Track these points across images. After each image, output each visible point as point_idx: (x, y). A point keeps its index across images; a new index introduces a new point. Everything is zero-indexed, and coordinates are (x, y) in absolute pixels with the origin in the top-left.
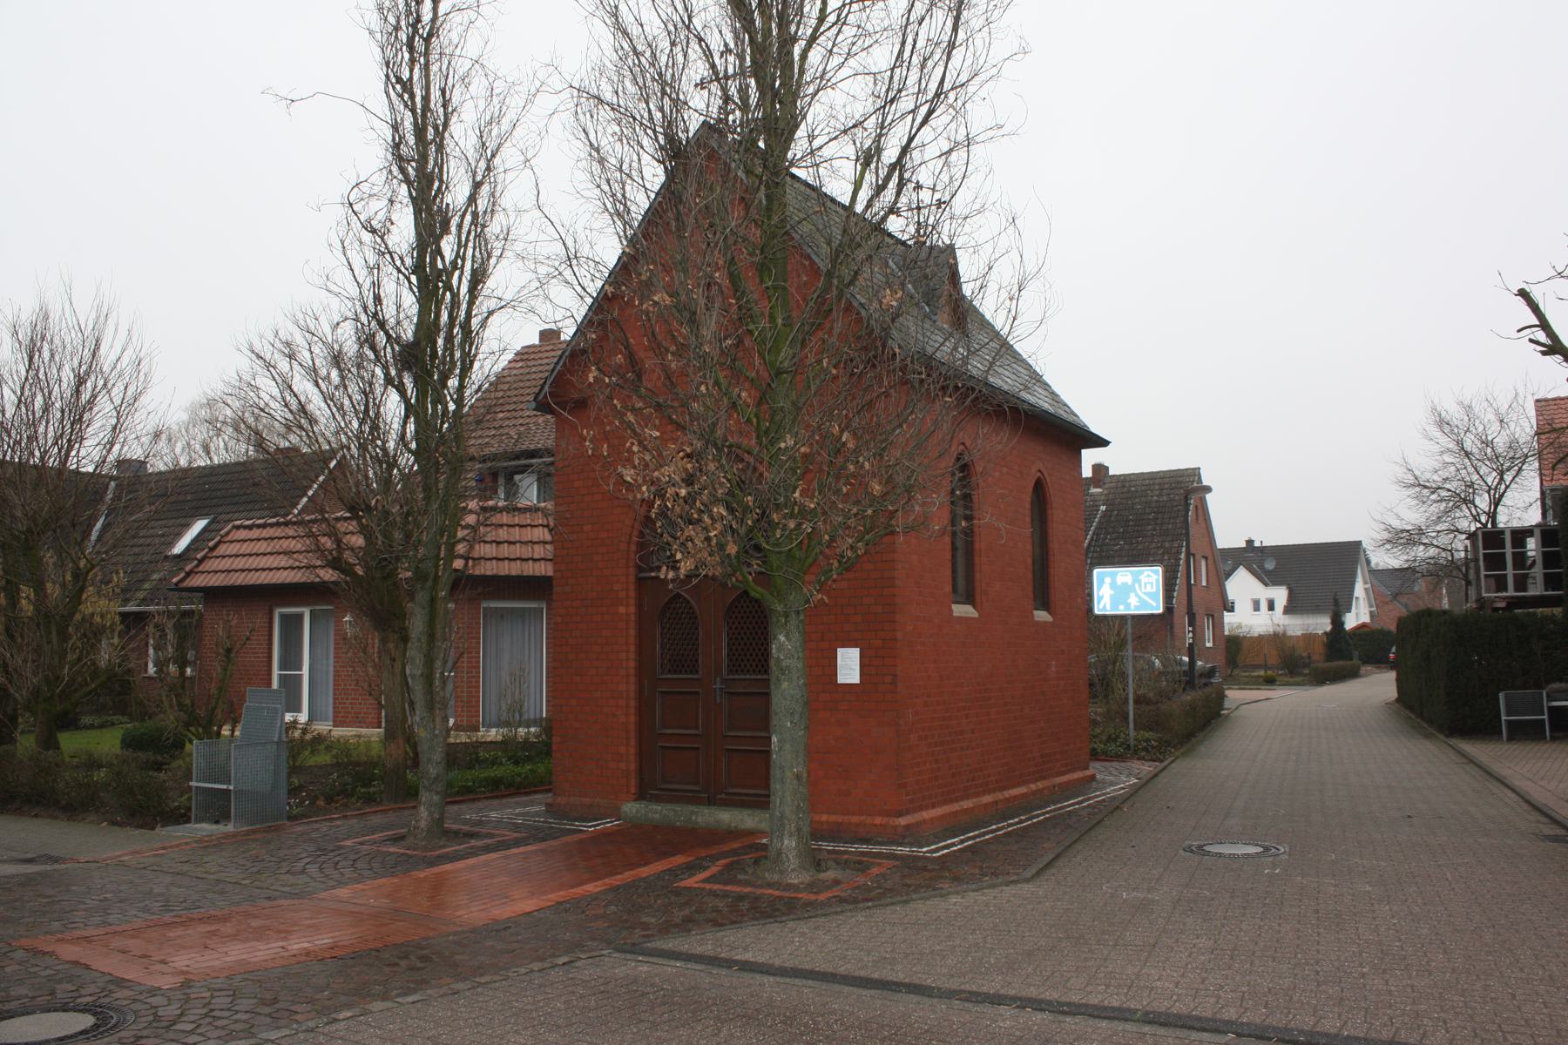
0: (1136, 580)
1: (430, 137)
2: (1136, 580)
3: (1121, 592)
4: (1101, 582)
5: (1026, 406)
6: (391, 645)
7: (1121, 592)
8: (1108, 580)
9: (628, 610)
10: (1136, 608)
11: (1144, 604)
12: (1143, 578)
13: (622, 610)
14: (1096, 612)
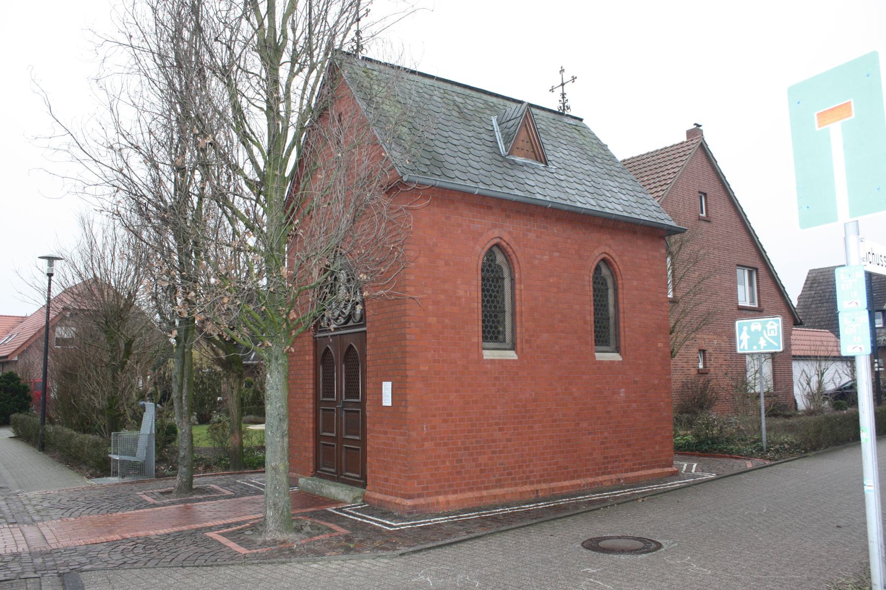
0: (764, 328)
1: (178, 106)
2: (764, 328)
3: (755, 337)
4: (741, 330)
5: (583, 211)
6: (231, 380)
7: (755, 337)
8: (745, 328)
9: (310, 358)
10: (765, 348)
11: (769, 344)
12: (768, 326)
13: (307, 358)
14: (739, 351)
